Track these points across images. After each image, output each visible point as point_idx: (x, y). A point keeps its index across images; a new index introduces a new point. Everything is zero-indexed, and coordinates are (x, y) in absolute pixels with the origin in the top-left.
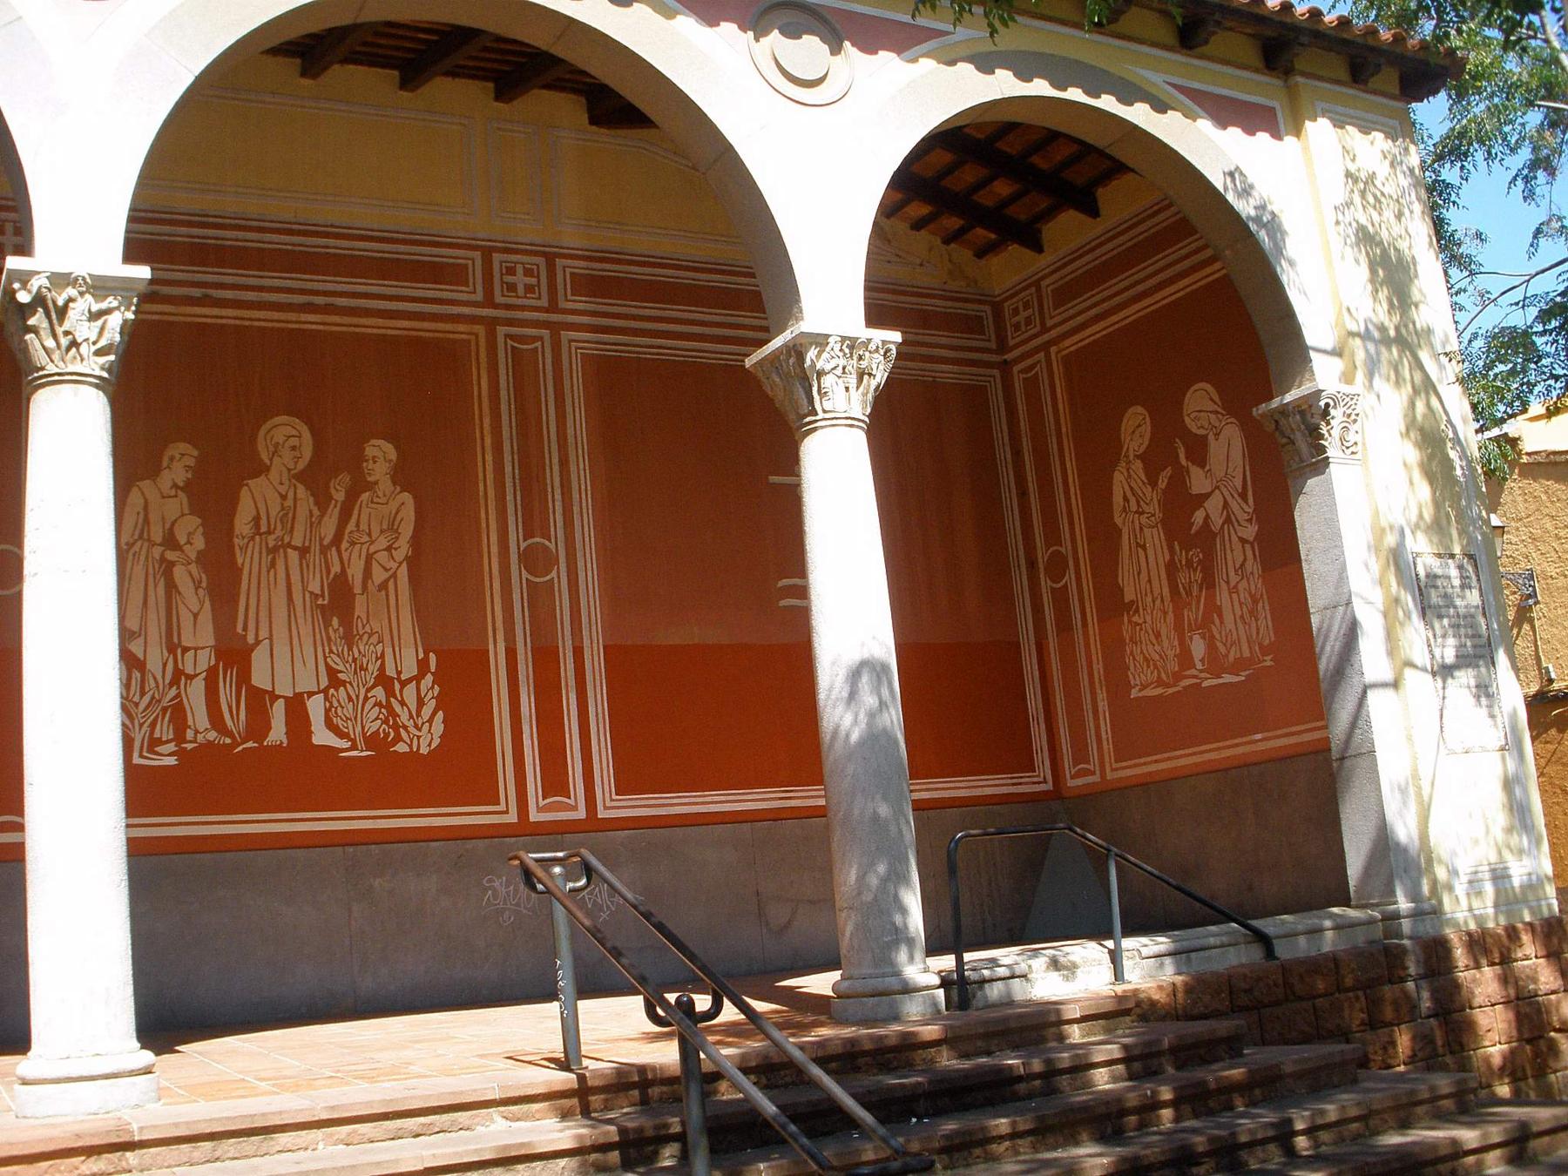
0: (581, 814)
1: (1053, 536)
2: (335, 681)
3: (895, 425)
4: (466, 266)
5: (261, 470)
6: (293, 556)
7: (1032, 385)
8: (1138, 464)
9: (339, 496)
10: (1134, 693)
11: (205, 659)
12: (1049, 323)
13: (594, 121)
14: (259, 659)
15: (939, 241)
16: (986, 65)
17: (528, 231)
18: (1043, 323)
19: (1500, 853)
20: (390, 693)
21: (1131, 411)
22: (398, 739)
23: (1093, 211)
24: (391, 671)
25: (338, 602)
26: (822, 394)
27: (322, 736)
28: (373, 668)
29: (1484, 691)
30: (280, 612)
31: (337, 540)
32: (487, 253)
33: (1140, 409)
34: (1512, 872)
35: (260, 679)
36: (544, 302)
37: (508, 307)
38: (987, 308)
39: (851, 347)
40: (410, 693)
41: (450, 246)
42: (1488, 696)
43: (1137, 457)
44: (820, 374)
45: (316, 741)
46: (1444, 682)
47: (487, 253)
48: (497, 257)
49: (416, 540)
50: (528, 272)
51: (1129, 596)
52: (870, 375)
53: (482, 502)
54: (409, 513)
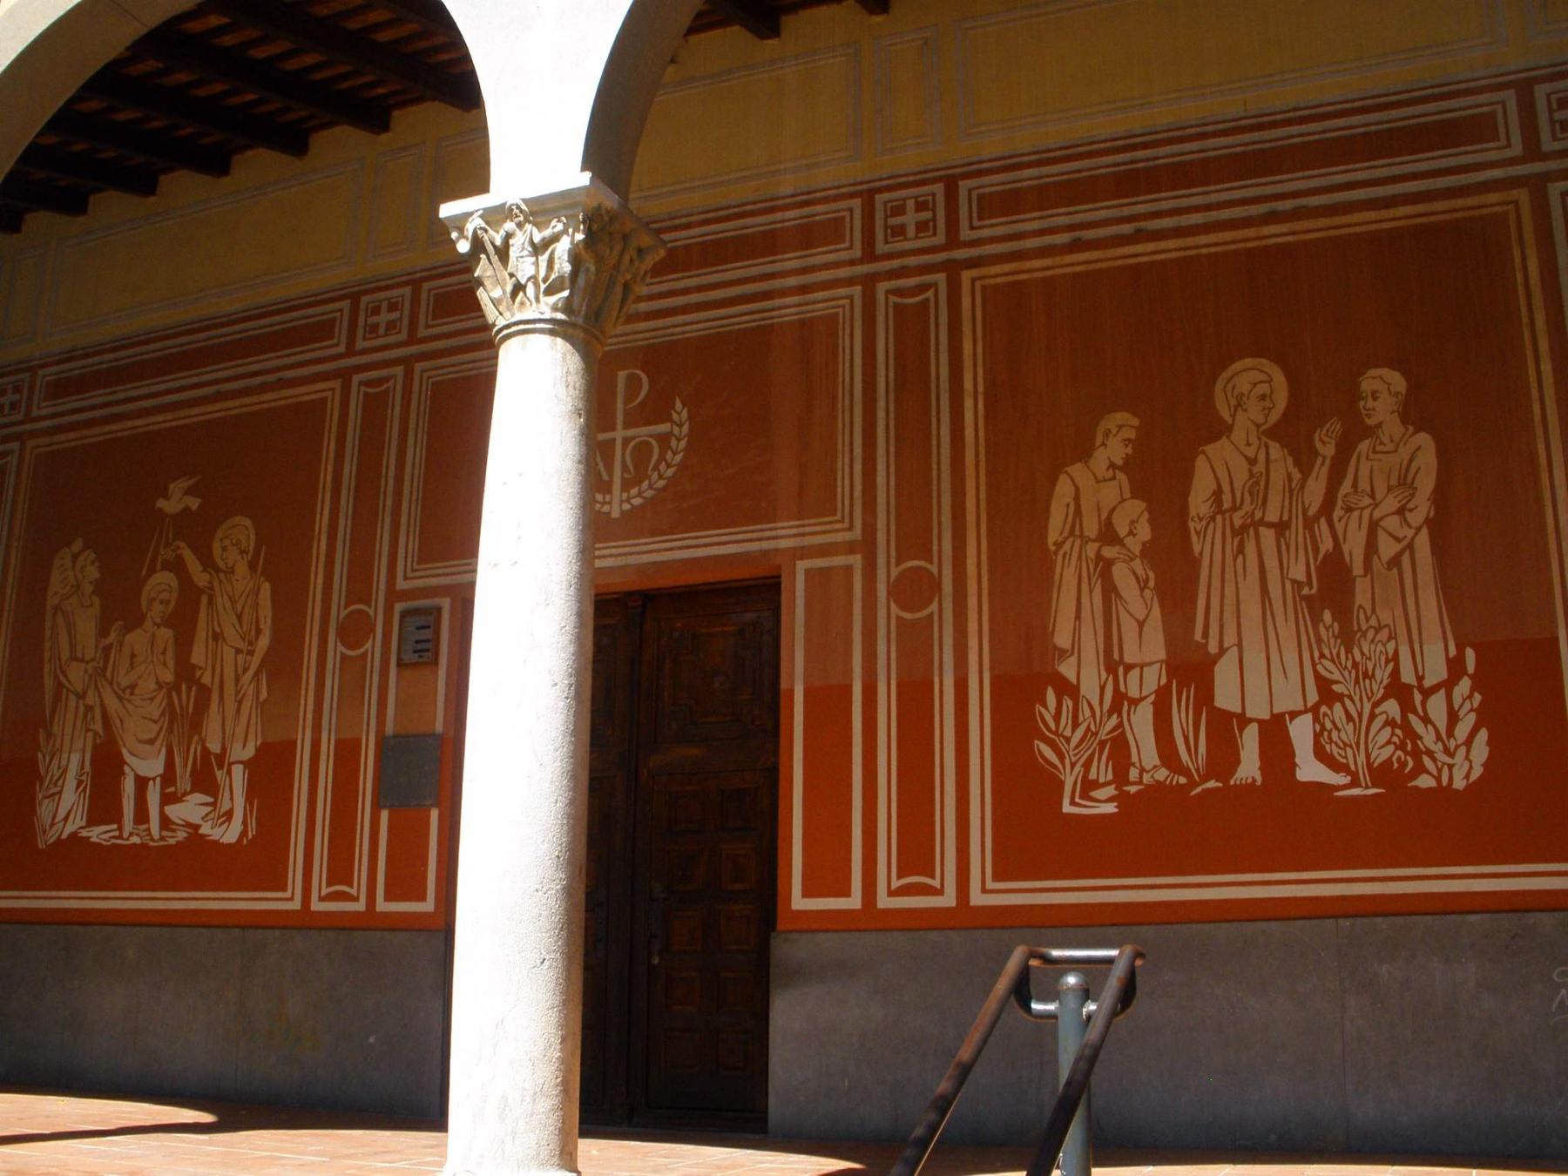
0: (948, 900)
2: (1327, 693)
5: (1219, 430)
6: (1268, 535)
9: (1328, 450)
11: (1153, 678)
12: (399, 370)
20: (1407, 707)
22: (1420, 769)
24: (1408, 677)
27: (1309, 770)
28: (1383, 675)
30: (1252, 609)
32: (868, 197)
35: (1225, 698)
40: (1437, 707)
49: (1440, 496)
53: (1539, 431)
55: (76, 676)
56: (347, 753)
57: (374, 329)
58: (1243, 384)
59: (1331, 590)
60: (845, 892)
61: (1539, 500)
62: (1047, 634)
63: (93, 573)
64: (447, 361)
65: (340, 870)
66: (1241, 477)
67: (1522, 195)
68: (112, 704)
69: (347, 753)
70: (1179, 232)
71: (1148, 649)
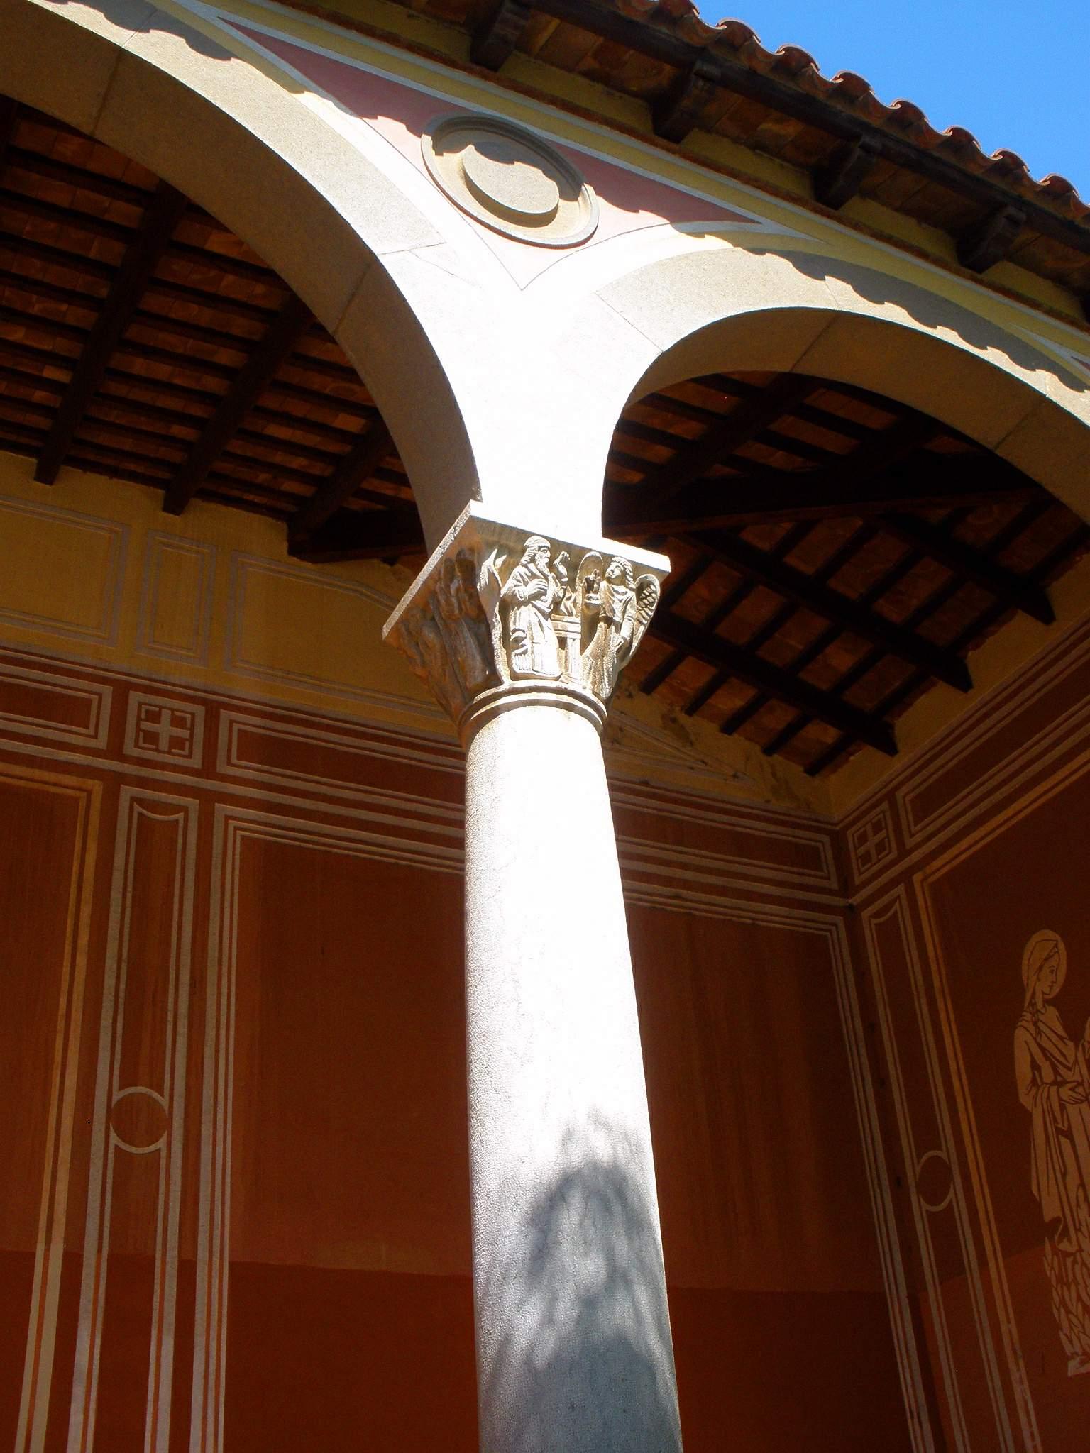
1: (927, 1134)
3: (654, 697)
4: (89, 701)
7: (889, 933)
8: (1052, 1012)
10: (1073, 1368)
12: (900, 889)
13: (292, 552)
15: (758, 748)
16: (813, 266)
17: (185, 669)
18: (901, 843)
21: (1036, 938)
23: (963, 682)
26: (511, 644)
32: (122, 690)
33: (1050, 934)
36: (196, 762)
37: (141, 762)
38: (826, 839)
39: (573, 567)
41: (69, 673)
43: (1047, 1002)
44: (508, 605)
47: (122, 690)
48: (135, 697)
50: (178, 722)
51: (1050, 1211)
52: (609, 621)
53: (61, 1025)
61: (46, 1093)
67: (97, 786)
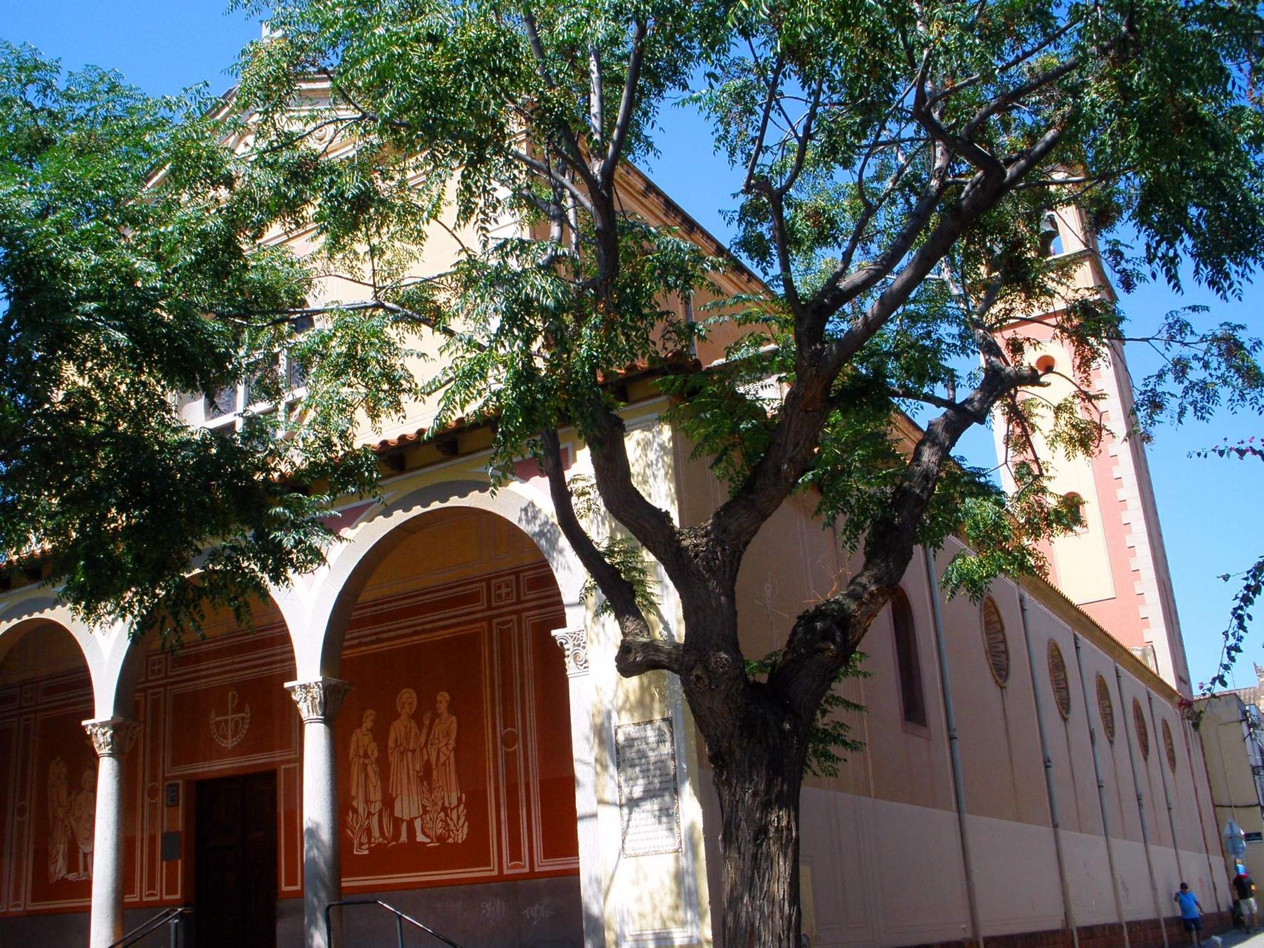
0: (527, 870)
2: (425, 812)
5: (398, 716)
6: (410, 754)
9: (427, 723)
11: (378, 806)
14: (397, 804)
19: (664, 923)
20: (446, 815)
22: (449, 836)
24: (447, 804)
25: (426, 775)
27: (420, 838)
28: (440, 803)
29: (667, 813)
30: (405, 781)
31: (426, 745)
32: (488, 581)
34: (675, 935)
35: (397, 814)
40: (454, 816)
42: (668, 815)
45: (418, 840)
46: (630, 813)
49: (458, 741)
54: (455, 726)
55: (61, 812)
56: (152, 839)
57: (153, 671)
58: (405, 697)
59: (426, 775)
60: (296, 884)
62: (349, 791)
63: (64, 770)
64: (549, 609)
65: (151, 886)
66: (403, 733)
68: (73, 823)
69: (152, 839)
70: (390, 639)
71: (376, 796)
